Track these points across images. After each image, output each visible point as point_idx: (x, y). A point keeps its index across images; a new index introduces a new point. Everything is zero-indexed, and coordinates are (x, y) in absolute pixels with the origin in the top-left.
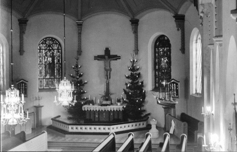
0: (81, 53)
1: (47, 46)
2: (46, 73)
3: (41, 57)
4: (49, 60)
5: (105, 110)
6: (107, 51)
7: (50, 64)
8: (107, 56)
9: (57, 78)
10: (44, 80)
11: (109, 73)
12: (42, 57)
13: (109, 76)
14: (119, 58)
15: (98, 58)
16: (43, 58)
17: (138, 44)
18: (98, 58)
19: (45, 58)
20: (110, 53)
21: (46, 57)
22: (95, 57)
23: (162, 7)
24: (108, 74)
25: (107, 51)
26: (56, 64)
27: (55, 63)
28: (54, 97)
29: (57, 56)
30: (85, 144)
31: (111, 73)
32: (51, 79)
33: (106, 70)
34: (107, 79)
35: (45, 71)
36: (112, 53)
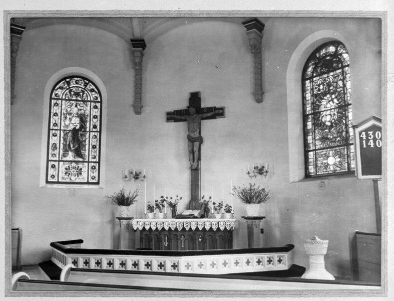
0: (135, 103)
1: (72, 93)
2: (66, 150)
3: (57, 115)
4: (73, 121)
5: (184, 229)
6: (195, 98)
7: (75, 131)
8: (194, 107)
9: (88, 162)
10: (61, 163)
11: (198, 145)
12: (59, 115)
13: (196, 154)
14: (221, 111)
15: (173, 116)
16: (62, 118)
17: (374, 201)
18: (173, 116)
19: (66, 118)
20: (200, 105)
21: (68, 117)
22: (168, 114)
23: (333, 46)
24: (196, 149)
25: (195, 98)
26: (90, 131)
27: (88, 130)
28: (49, 188)
29: (92, 116)
30: (76, 289)
31: (203, 147)
32: (77, 162)
33: (191, 140)
34: (194, 161)
35: (65, 145)
36: (204, 105)
